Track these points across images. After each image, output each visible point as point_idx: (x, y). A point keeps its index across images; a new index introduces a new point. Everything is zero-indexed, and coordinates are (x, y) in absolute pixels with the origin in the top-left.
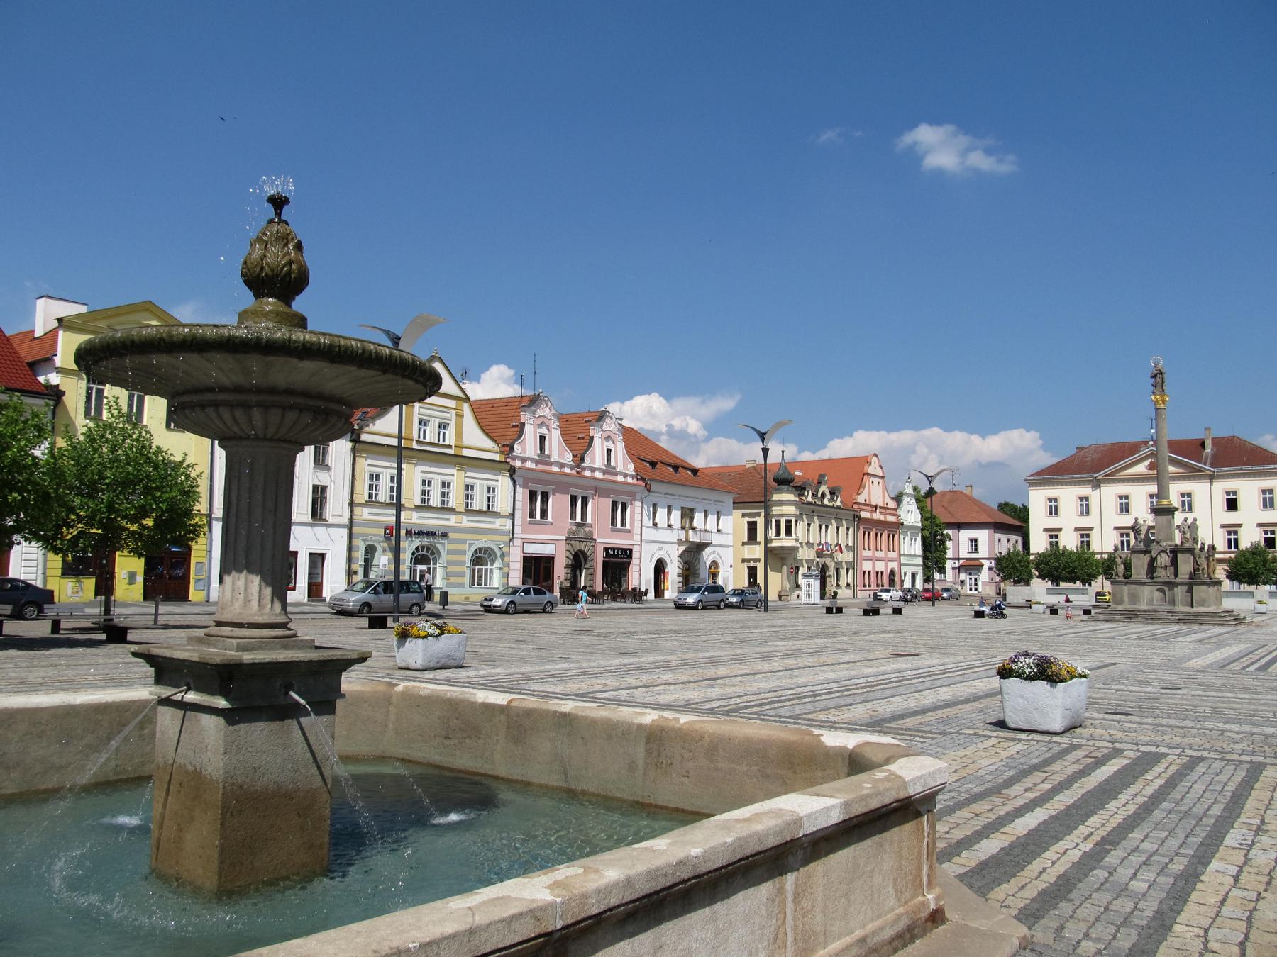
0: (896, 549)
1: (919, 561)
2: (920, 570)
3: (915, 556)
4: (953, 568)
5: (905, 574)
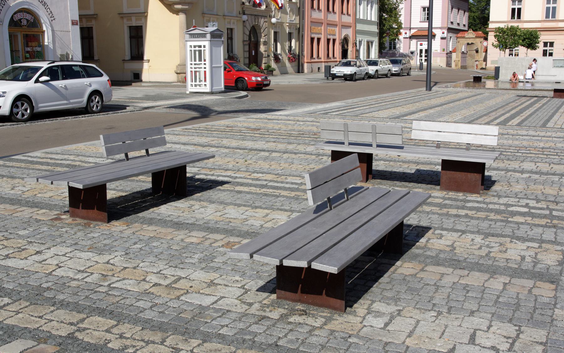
0: (350, 12)
1: (375, 29)
2: (376, 41)
3: (370, 23)
4: (442, 38)
5: (360, 42)
